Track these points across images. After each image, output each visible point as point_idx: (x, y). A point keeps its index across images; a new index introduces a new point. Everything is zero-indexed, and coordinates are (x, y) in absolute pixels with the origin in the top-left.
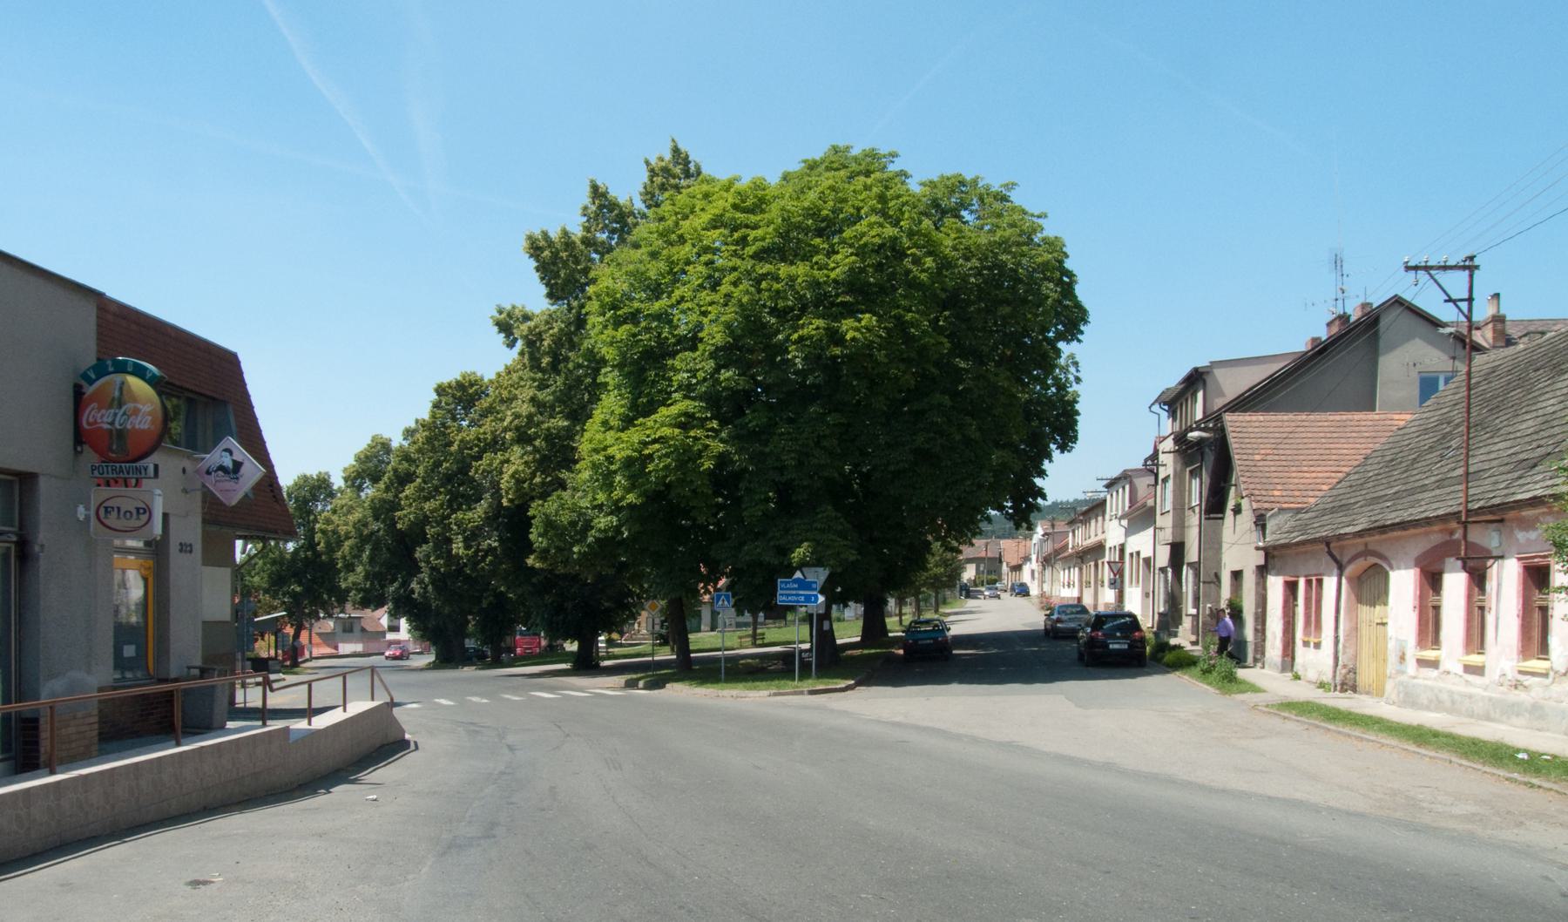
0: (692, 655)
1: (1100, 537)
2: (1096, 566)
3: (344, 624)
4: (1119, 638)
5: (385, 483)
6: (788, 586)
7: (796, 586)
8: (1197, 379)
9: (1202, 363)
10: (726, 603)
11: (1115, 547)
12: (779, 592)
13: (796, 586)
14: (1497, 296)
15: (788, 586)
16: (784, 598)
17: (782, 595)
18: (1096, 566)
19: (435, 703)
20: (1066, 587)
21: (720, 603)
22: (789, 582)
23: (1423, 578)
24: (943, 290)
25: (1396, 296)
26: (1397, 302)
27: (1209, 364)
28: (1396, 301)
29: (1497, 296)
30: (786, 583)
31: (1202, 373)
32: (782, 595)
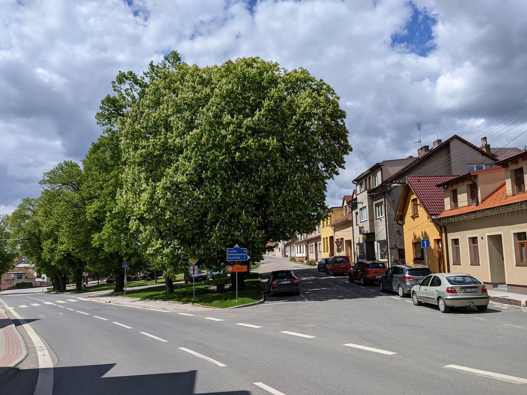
0: (173, 283)
1: (319, 234)
2: (316, 245)
3: (18, 276)
4: (380, 263)
5: (124, 94)
6: (232, 252)
7: (236, 251)
8: (377, 168)
9: (380, 161)
10: (127, 265)
11: (327, 238)
12: (228, 254)
13: (236, 251)
14: (485, 138)
15: (232, 252)
16: (230, 258)
17: (229, 256)
18: (316, 245)
19: (224, 319)
20: (299, 253)
21: (125, 265)
22: (232, 250)
23: (489, 239)
24: (160, 150)
25: (456, 135)
26: (456, 137)
27: (382, 162)
28: (456, 137)
29: (485, 138)
30: (231, 250)
31: (380, 165)
32: (229, 256)
